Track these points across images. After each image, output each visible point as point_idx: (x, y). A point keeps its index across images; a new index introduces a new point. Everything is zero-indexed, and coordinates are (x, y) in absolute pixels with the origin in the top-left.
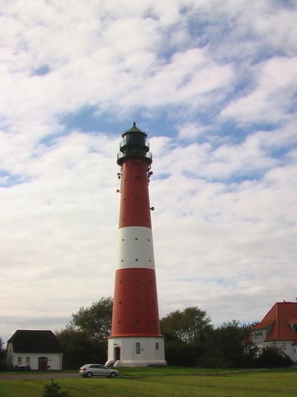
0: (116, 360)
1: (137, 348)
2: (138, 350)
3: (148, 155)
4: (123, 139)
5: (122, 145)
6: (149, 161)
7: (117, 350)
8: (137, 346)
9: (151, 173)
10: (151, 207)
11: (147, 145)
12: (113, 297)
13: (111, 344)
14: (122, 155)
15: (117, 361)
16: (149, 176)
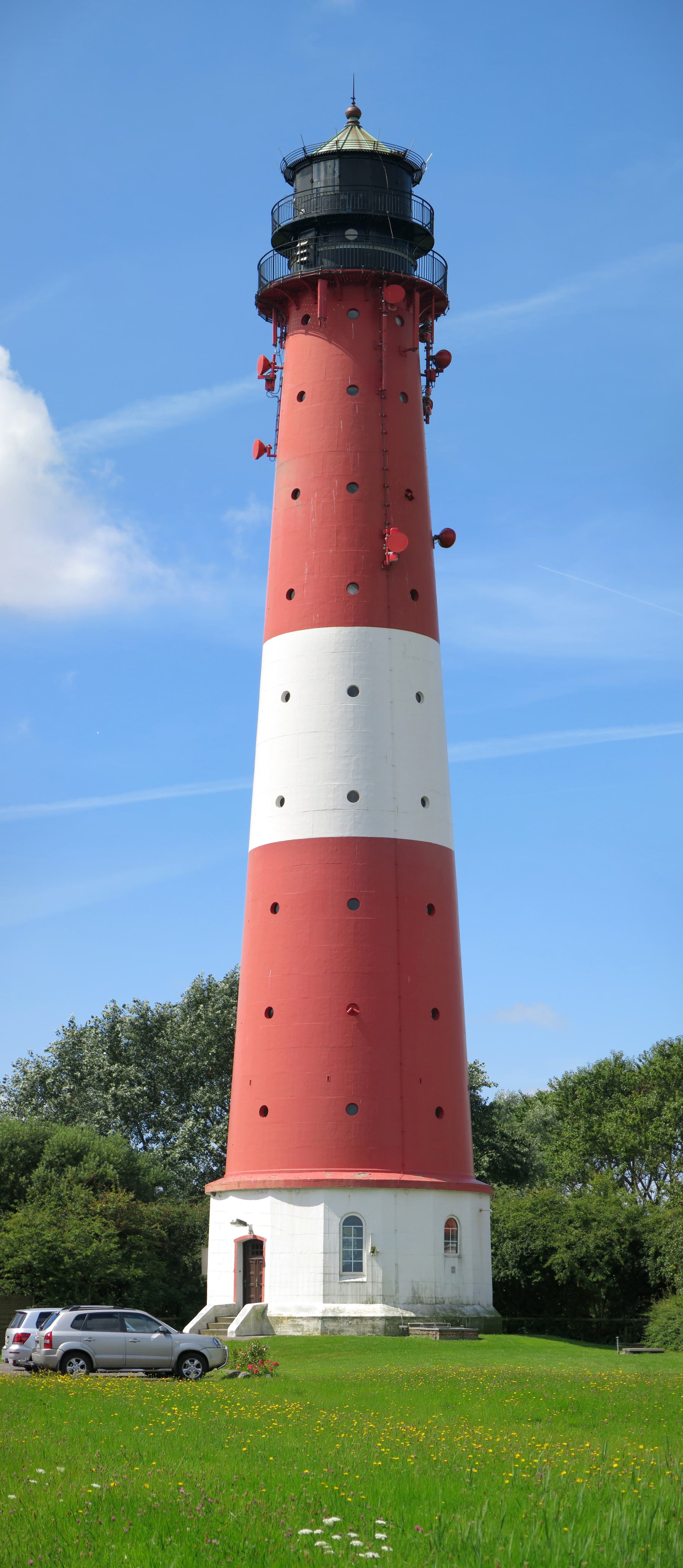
0: (245, 1303)
1: (345, 1243)
2: (350, 1249)
3: (424, 270)
4: (290, 190)
5: (287, 218)
6: (434, 300)
7: (252, 1251)
8: (345, 1233)
9: (442, 360)
10: (436, 530)
11: (417, 216)
12: (480, 1094)
13: (228, 1219)
14: (281, 269)
15: (249, 1307)
16: (431, 377)
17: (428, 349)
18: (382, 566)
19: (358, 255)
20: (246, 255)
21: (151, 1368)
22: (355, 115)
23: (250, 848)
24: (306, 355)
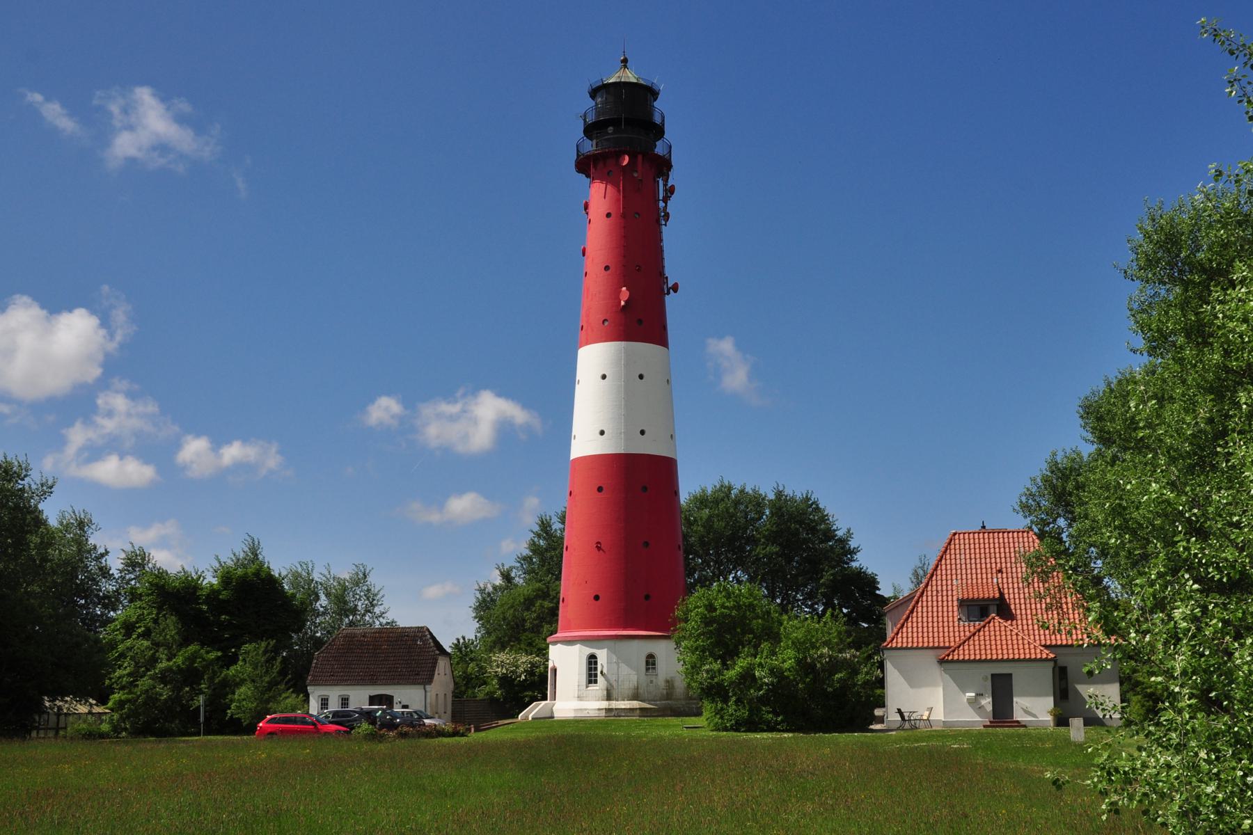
3: (660, 149)
4: (593, 103)
5: (591, 119)
11: (657, 120)
14: (589, 147)
16: (665, 200)
17: (665, 185)
18: (639, 313)
19: (625, 138)
20: (570, 137)
21: (283, 731)
22: (625, 61)
23: (572, 457)
24: (599, 196)
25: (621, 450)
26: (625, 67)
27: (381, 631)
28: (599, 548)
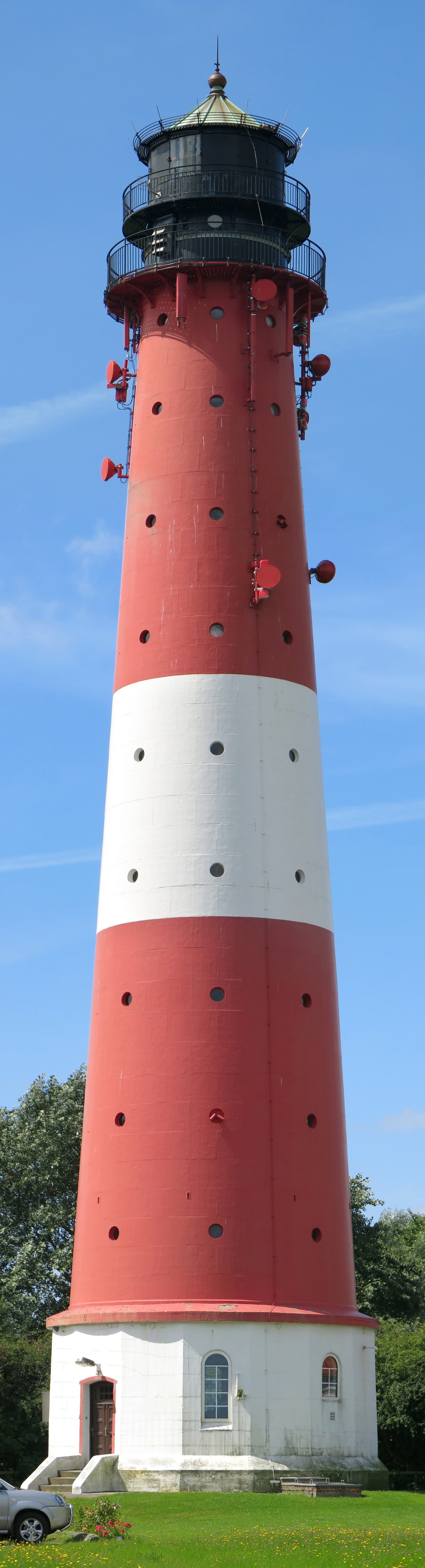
3: (299, 262)
4: (145, 170)
5: (140, 202)
11: (291, 200)
14: (134, 261)
16: (306, 385)
17: (303, 353)
18: (250, 607)
20: (93, 246)
22: (219, 83)
23: (100, 929)
24: (163, 361)
25: (209, 914)
26: (221, 93)
27: (128, 282)
28: (277, 407)
